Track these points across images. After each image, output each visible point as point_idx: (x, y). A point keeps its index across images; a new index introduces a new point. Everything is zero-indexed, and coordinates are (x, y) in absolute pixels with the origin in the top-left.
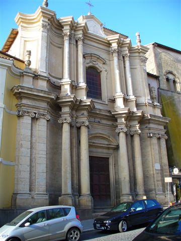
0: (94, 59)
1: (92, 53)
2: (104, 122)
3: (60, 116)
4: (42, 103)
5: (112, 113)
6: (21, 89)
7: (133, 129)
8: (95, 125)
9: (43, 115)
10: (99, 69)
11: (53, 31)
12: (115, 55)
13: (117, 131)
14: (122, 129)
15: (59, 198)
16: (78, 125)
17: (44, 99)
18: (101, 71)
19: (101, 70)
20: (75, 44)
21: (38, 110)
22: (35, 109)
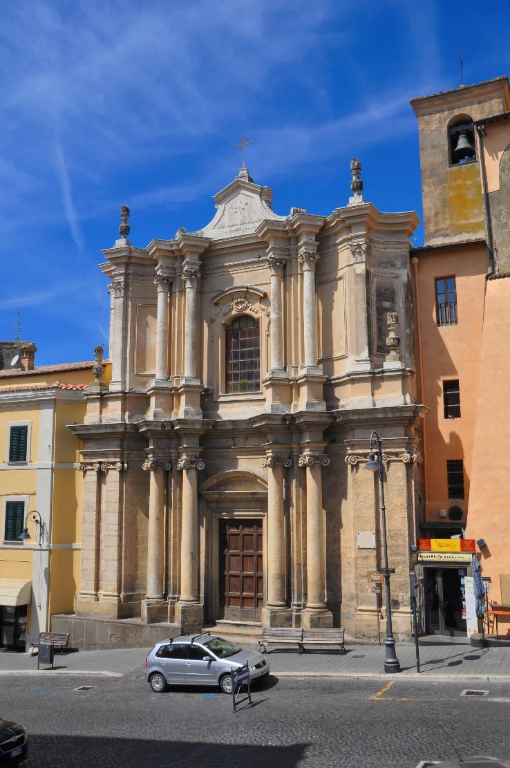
18: (258, 320)
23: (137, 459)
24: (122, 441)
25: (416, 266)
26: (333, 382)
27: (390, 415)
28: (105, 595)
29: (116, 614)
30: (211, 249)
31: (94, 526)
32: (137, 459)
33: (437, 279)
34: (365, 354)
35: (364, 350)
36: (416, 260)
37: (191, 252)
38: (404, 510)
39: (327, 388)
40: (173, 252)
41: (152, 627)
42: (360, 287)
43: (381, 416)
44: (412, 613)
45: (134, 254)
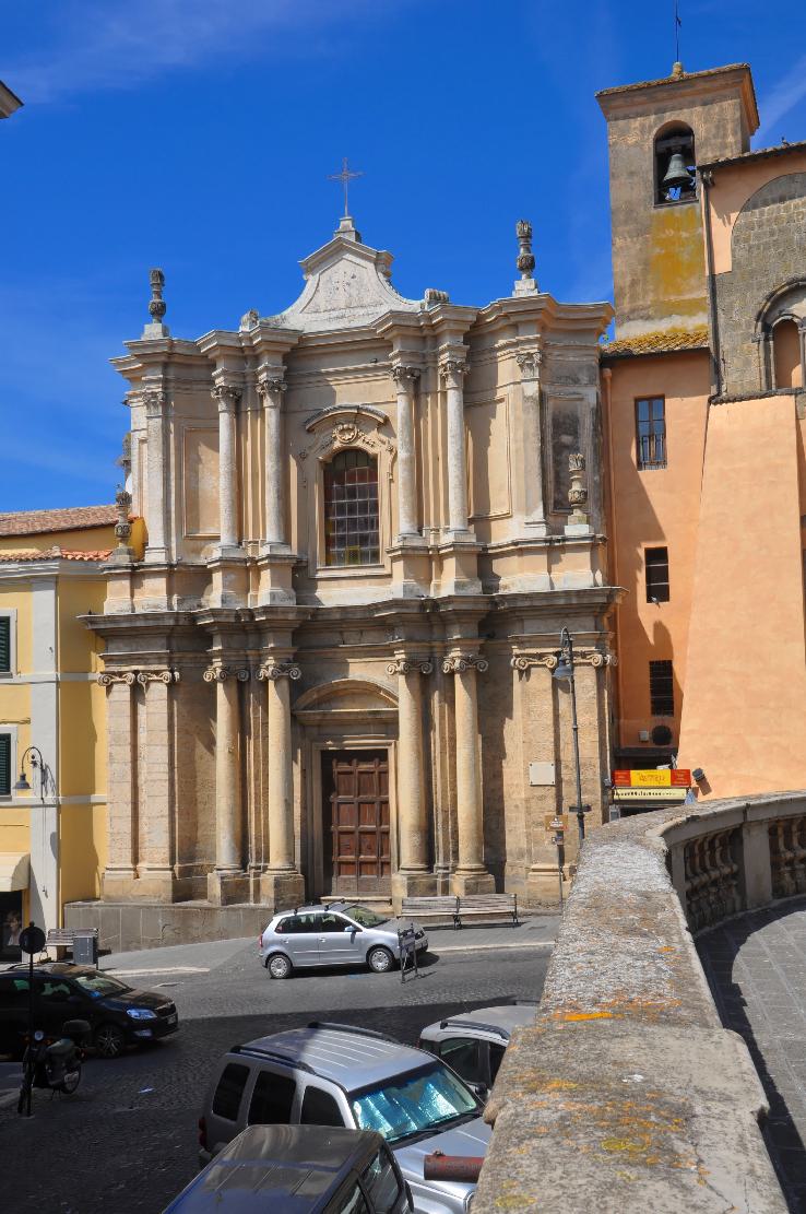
25: (609, 381)
31: (128, 768)
33: (637, 400)
34: (538, 514)
35: (537, 507)
36: (608, 372)
39: (482, 561)
45: (177, 350)
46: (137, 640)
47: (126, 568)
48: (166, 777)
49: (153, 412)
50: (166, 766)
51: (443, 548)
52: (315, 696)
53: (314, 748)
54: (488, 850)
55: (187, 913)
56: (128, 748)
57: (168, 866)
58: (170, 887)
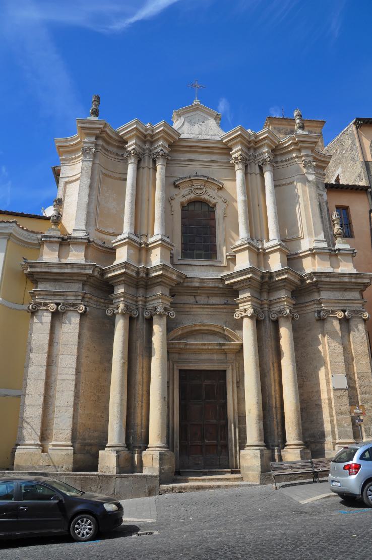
0: (197, 184)
1: (210, 176)
2: (215, 300)
3: (111, 302)
4: (72, 285)
5: (227, 282)
6: (31, 267)
7: (276, 308)
8: (192, 310)
9: (73, 305)
10: (211, 203)
11: (111, 153)
12: (151, 170)
13: (237, 316)
14: (245, 311)
15: (101, 452)
16: (274, 317)
17: (75, 278)
18: (215, 205)
19: (213, 201)
20: (151, 165)
21: (62, 297)
22: (58, 297)
23: (95, 306)
24: (83, 284)
26: (301, 255)
27: (353, 280)
28: (54, 445)
29: (71, 466)
30: (175, 144)
31: (44, 370)
32: (95, 306)
34: (322, 236)
35: (320, 234)
37: (166, 140)
38: (366, 356)
39: (292, 259)
40: (145, 136)
41: (122, 477)
42: (313, 190)
43: (347, 280)
44: (72, 446)
45: (107, 130)
46: (60, 283)
47: (59, 238)
48: (74, 377)
49: (88, 158)
50: (74, 370)
51: (267, 249)
52: (180, 333)
53: (175, 367)
54: (13, 499)
55: (86, 479)
56: (45, 356)
57: (69, 443)
58: (71, 460)
